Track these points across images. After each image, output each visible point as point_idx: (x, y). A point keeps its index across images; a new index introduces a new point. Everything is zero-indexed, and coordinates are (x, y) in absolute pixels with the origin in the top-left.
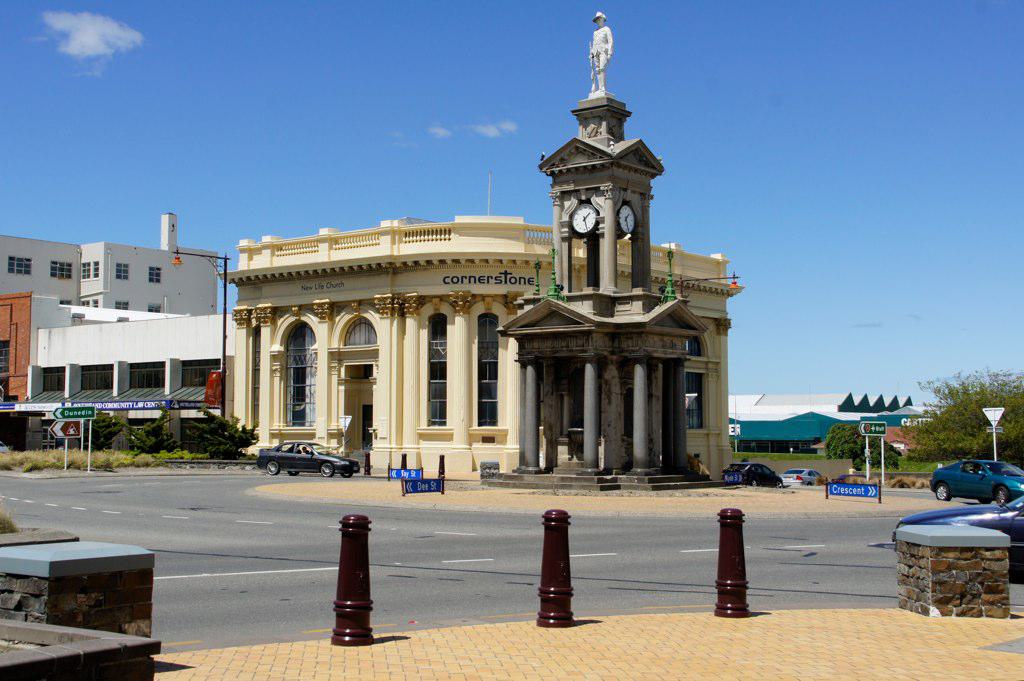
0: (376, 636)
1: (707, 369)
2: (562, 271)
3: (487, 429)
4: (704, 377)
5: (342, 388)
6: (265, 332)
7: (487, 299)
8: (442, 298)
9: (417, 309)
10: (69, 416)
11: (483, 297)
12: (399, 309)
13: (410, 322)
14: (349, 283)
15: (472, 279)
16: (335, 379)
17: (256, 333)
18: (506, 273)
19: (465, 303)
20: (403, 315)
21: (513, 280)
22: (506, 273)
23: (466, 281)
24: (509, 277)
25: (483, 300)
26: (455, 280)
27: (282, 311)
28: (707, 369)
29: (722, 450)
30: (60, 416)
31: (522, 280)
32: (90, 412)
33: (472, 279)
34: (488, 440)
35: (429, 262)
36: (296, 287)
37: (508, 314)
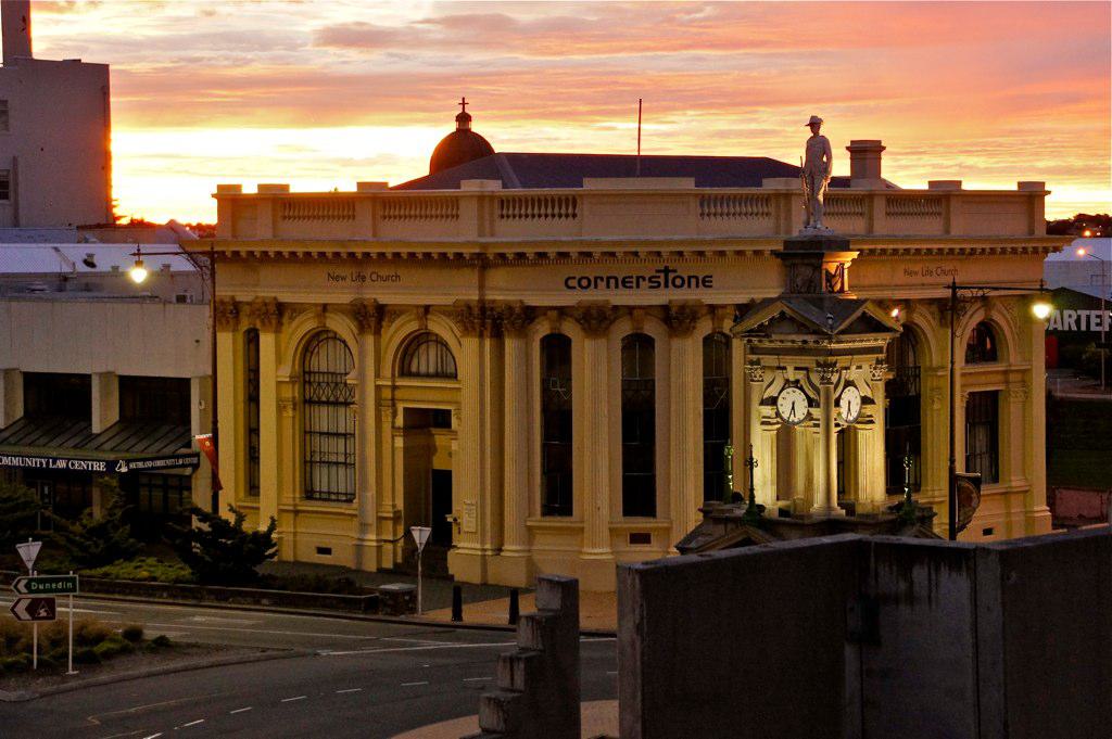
0: (453, 371)
1: (1007, 382)
2: (595, 554)
3: (640, 524)
4: (1001, 397)
5: (399, 442)
6: (267, 341)
7: (635, 312)
8: (562, 312)
9: (522, 326)
10: (38, 591)
11: (630, 309)
12: (490, 322)
13: (511, 345)
14: (410, 276)
15: (612, 281)
16: (387, 426)
17: (252, 339)
18: (666, 271)
19: (596, 320)
20: (498, 335)
21: (678, 282)
22: (666, 271)
23: (602, 284)
24: (671, 276)
25: (631, 314)
26: (584, 283)
27: (294, 311)
28: (1007, 382)
29: (1034, 519)
30: (24, 590)
31: (693, 281)
32: (70, 585)
33: (612, 281)
34: (641, 538)
35: (542, 256)
36: (319, 274)
37: (670, 336)
